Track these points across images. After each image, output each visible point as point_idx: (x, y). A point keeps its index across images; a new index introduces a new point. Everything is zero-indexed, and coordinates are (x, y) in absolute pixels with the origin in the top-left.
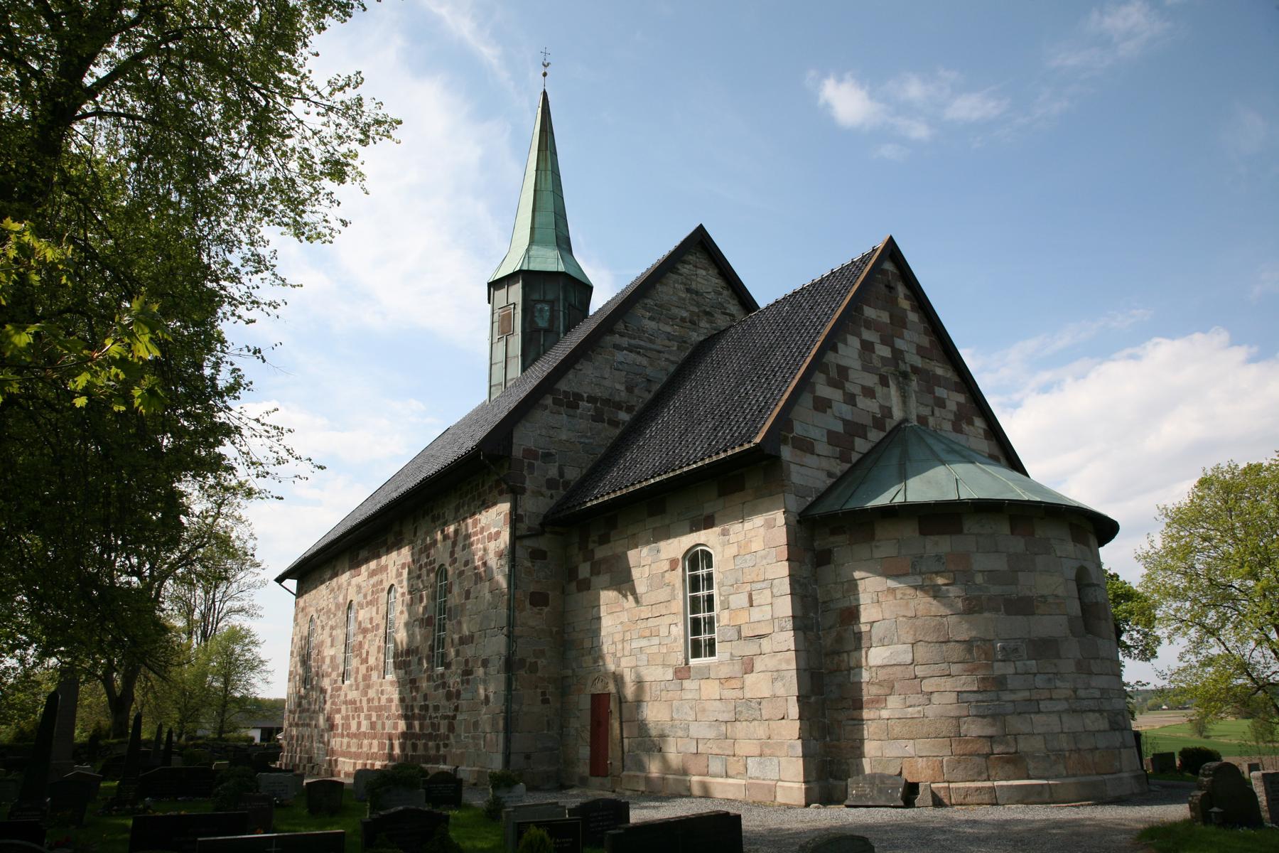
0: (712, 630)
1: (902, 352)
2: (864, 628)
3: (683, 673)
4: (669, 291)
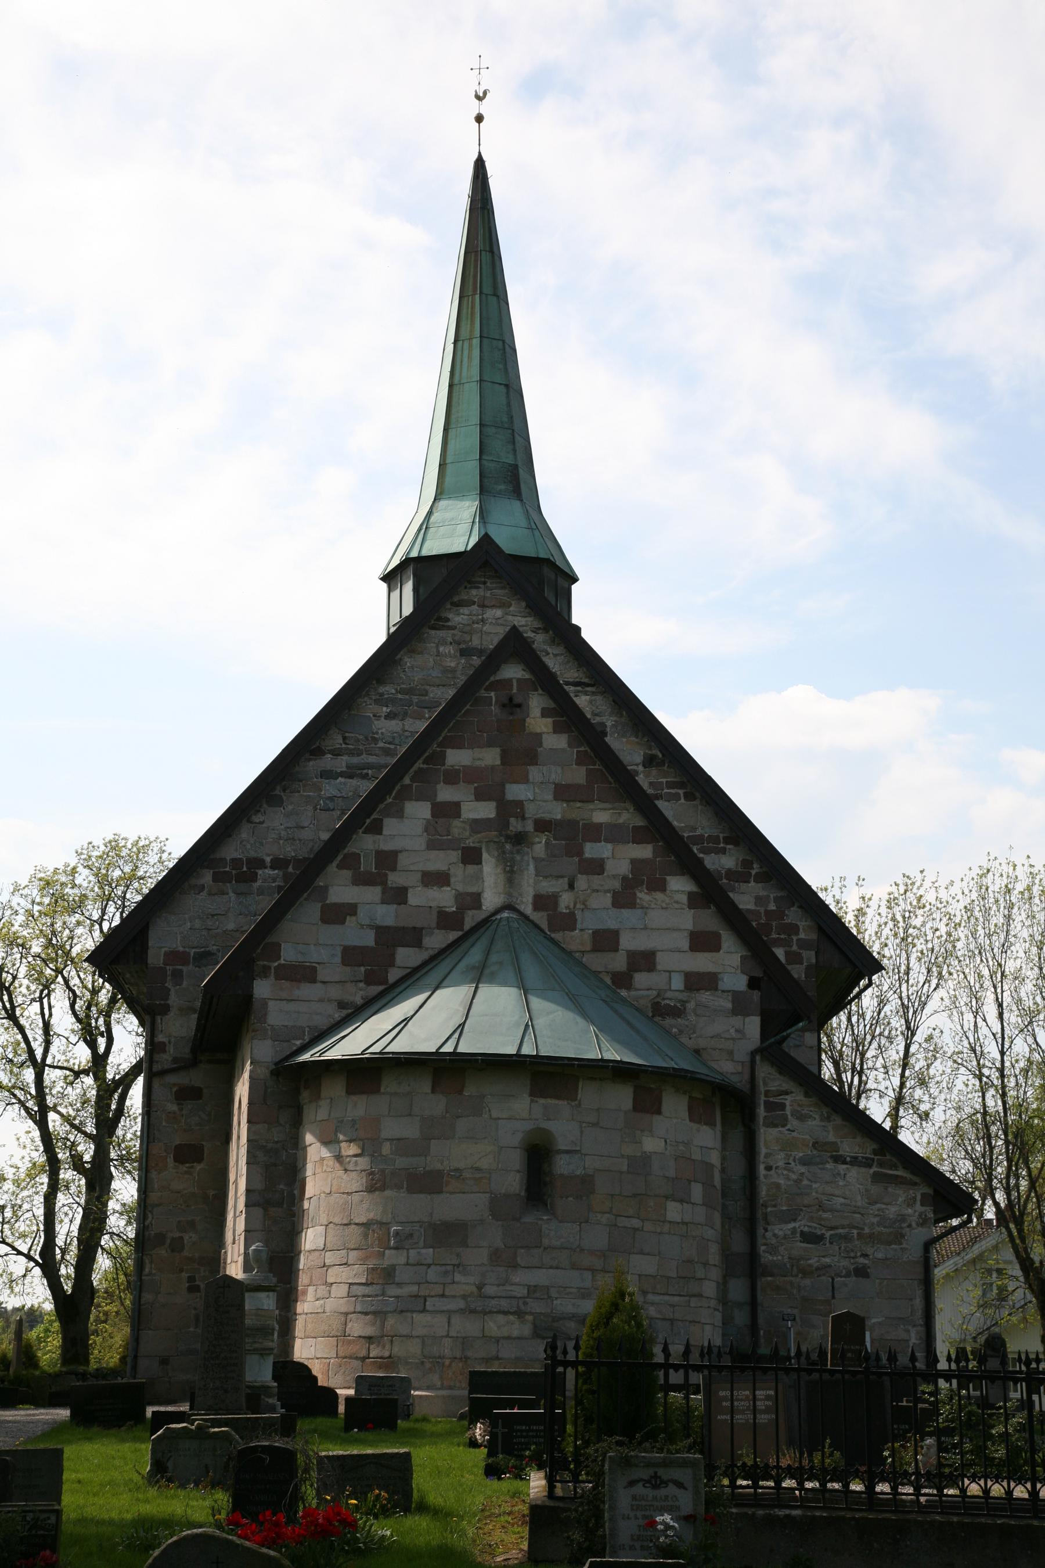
1: (520, 804)
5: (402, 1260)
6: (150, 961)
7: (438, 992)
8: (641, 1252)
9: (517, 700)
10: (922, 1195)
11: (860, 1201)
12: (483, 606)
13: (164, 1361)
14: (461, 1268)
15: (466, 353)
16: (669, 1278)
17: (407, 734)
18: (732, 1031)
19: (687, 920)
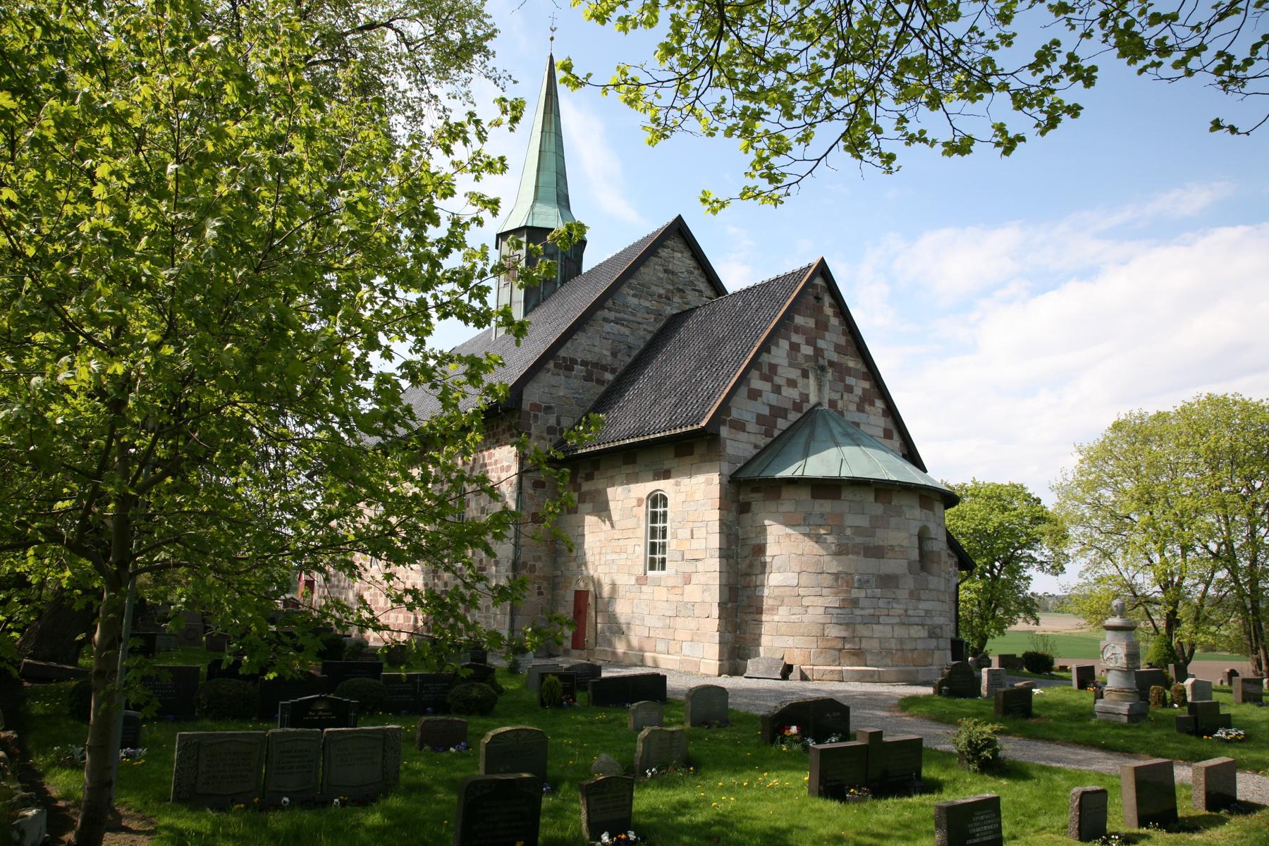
0: (664, 552)
1: (822, 350)
2: (768, 559)
3: (642, 581)
4: (650, 273)
5: (863, 595)
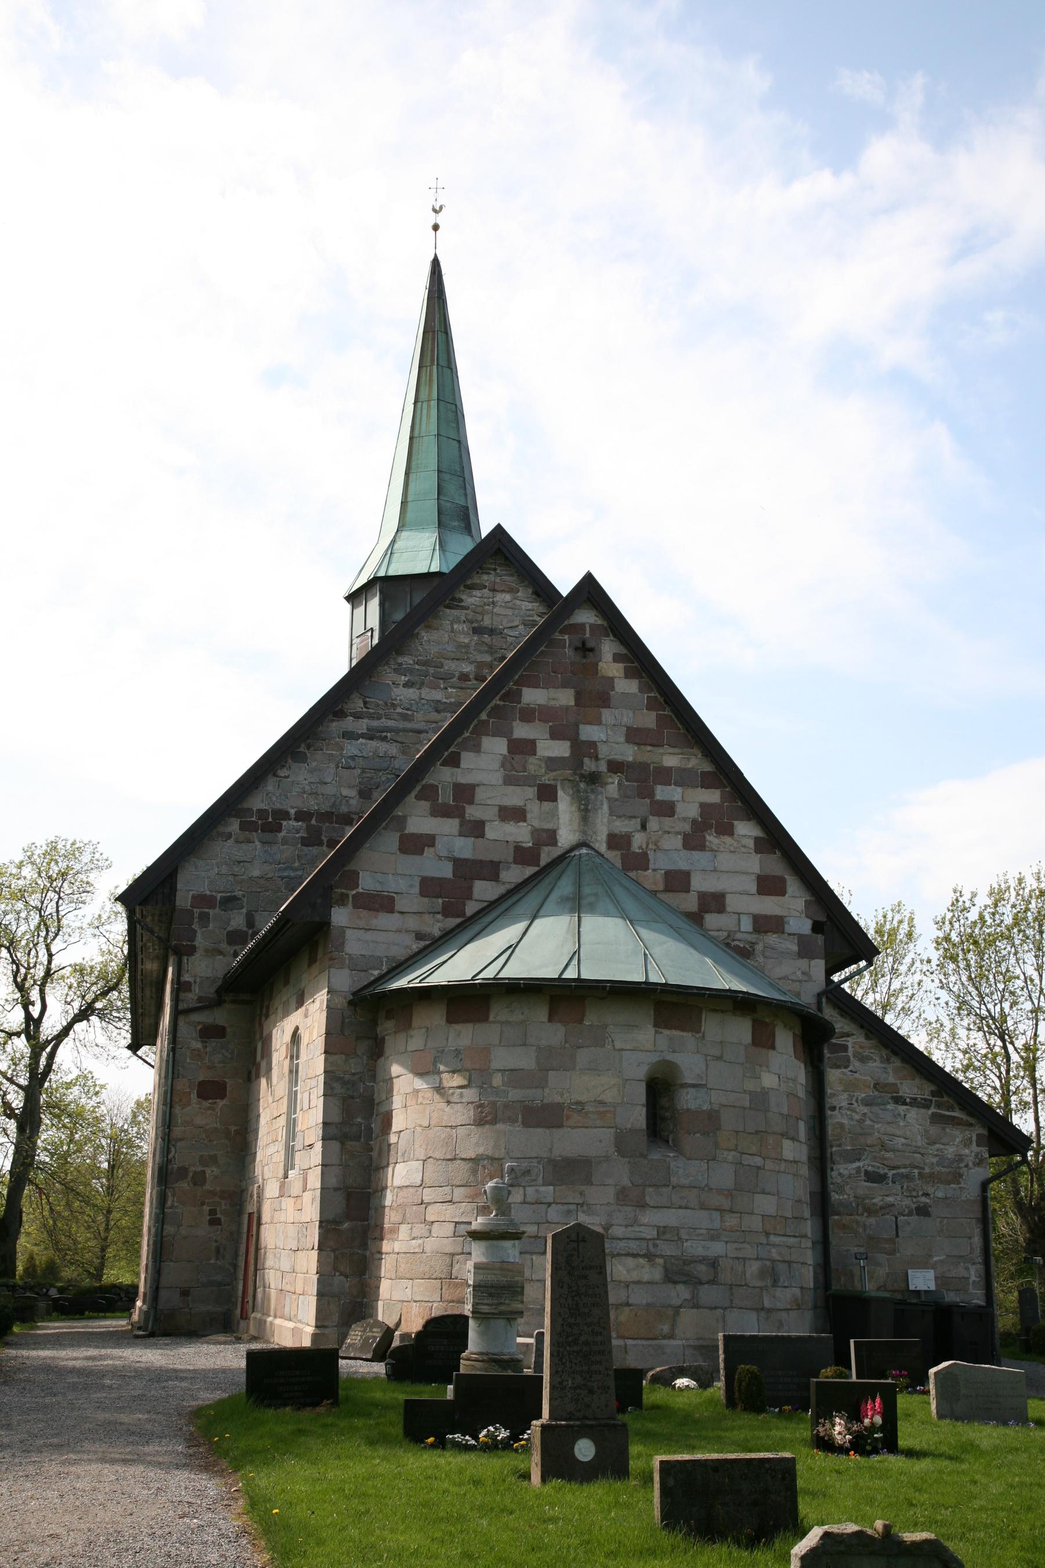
1: (593, 745)
6: (178, 903)
7: (537, 922)
8: (763, 1192)
9: (589, 645)
10: (977, 1135)
11: (920, 1141)
12: (493, 590)
13: (185, 1293)
14: (585, 1208)
15: (425, 411)
16: (786, 1218)
17: (423, 701)
18: (799, 973)
19: (754, 864)
